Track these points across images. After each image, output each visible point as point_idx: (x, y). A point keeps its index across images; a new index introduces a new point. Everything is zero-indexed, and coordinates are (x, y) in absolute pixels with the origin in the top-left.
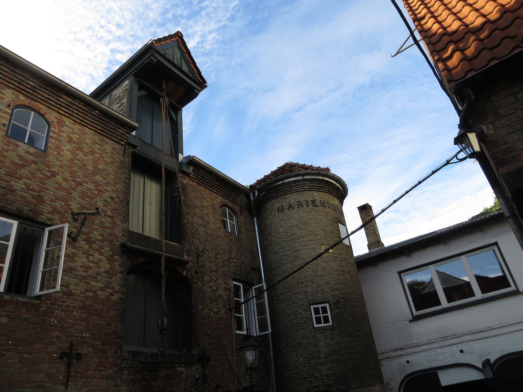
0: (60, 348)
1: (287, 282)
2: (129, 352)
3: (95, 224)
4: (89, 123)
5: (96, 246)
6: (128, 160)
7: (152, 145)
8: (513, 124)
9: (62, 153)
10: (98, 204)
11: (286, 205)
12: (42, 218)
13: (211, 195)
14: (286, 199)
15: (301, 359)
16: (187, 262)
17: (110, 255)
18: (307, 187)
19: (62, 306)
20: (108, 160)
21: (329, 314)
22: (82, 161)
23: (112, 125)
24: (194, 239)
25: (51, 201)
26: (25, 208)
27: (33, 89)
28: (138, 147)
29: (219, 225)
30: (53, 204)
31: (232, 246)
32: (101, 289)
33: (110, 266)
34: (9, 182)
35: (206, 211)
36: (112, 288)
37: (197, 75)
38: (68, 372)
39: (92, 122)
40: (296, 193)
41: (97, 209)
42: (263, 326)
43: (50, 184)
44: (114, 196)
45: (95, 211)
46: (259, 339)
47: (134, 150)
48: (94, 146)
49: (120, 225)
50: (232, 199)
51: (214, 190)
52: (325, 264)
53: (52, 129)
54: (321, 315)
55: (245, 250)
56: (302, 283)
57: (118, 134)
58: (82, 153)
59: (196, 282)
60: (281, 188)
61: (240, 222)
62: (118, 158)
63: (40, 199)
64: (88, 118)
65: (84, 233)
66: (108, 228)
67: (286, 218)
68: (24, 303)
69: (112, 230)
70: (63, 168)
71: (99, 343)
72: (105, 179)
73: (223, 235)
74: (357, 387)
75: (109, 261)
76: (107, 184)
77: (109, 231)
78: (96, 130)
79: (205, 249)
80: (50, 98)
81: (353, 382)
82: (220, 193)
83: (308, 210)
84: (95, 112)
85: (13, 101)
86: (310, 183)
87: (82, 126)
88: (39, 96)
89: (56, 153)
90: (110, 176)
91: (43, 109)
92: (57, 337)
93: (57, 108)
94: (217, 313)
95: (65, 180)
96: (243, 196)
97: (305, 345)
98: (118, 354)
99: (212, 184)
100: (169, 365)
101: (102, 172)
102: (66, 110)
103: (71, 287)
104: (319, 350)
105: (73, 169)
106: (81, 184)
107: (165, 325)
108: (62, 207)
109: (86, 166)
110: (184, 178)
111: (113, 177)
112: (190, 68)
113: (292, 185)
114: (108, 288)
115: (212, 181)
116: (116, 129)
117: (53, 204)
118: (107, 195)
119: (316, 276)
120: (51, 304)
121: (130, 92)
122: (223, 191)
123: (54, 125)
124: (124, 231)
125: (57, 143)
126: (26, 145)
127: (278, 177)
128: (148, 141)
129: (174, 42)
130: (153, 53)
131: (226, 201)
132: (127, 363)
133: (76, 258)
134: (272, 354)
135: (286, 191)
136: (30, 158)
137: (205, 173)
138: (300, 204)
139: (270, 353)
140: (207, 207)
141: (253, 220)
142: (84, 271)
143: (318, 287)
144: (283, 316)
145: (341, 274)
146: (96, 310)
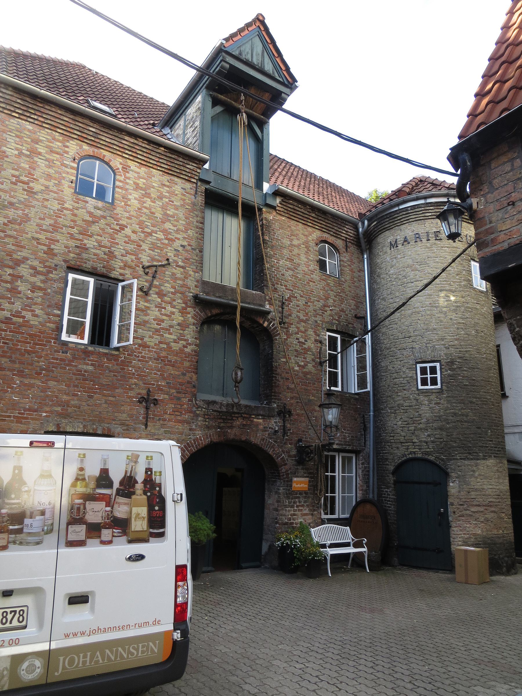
0: (139, 394)
1: (393, 335)
2: (203, 401)
3: (167, 276)
4: (155, 163)
5: (169, 299)
6: (201, 199)
7: (230, 178)
8: (502, 200)
9: (129, 203)
10: (169, 254)
11: (400, 238)
12: (114, 274)
13: (305, 230)
14: (401, 230)
15: (400, 423)
16: (268, 313)
17: (183, 307)
18: (430, 214)
19: (138, 357)
20: (178, 204)
21: (438, 375)
22: (149, 209)
23: (180, 161)
24: (279, 286)
25: (122, 255)
26: (99, 265)
27: (95, 135)
28: (211, 182)
29: (314, 266)
30: (124, 258)
31: (329, 292)
32: (175, 341)
33: (182, 319)
34: (82, 241)
35: (296, 251)
36: (185, 340)
37: (285, 73)
38: (147, 414)
39: (158, 161)
40: (415, 222)
41: (168, 260)
42: (362, 383)
43: (120, 238)
44: (185, 243)
45: (166, 262)
46: (357, 397)
47: (208, 187)
48: (162, 190)
49: (193, 276)
50: (334, 233)
51: (309, 224)
52: (442, 315)
53: (118, 177)
54: (429, 376)
55: (346, 295)
56: (409, 337)
57: (188, 170)
58: (149, 200)
59: (279, 334)
60: (396, 216)
61: (343, 261)
62: (189, 199)
63: (111, 255)
64: (153, 158)
65: (156, 287)
66: (180, 279)
67: (399, 256)
68: (106, 354)
69: (184, 281)
70: (130, 219)
71: (174, 391)
72: (175, 226)
73: (318, 278)
74: (461, 459)
75: (182, 313)
76: (178, 231)
77: (181, 282)
78: (163, 170)
79: (292, 297)
80: (113, 142)
81: (456, 453)
82: (317, 227)
83: (428, 245)
84: (160, 149)
85: (77, 153)
86: (435, 208)
87: (149, 168)
88: (102, 142)
89: (123, 203)
90: (181, 222)
91: (108, 156)
92: (136, 384)
93: (120, 152)
94: (303, 367)
95: (134, 232)
96: (349, 227)
97: (406, 408)
98: (192, 402)
99: (306, 216)
100: (246, 415)
101: (171, 219)
102: (130, 153)
103: (146, 339)
104: (421, 415)
105: (141, 219)
106: (150, 234)
107: (239, 378)
108: (132, 261)
109: (153, 213)
110: (269, 213)
111: (184, 223)
112: (275, 66)
113: (410, 212)
114: (182, 340)
115: (307, 212)
116: (185, 165)
117: (124, 258)
118: (177, 244)
119: (427, 330)
120: (128, 355)
121: (202, 110)
122: (321, 224)
123: (120, 172)
124: (197, 281)
125: (124, 192)
126: (94, 200)
127: (392, 203)
128: (226, 173)
129: (253, 32)
130: (223, 57)
131: (326, 236)
132: (201, 411)
133: (148, 312)
134: (372, 413)
135: (402, 220)
136: (99, 213)
137: (296, 204)
138: (418, 237)
139: (369, 412)
140: (298, 246)
141: (363, 257)
142: (157, 324)
143: (429, 343)
144: (385, 374)
145: (462, 328)
146: (170, 361)
